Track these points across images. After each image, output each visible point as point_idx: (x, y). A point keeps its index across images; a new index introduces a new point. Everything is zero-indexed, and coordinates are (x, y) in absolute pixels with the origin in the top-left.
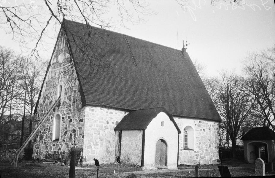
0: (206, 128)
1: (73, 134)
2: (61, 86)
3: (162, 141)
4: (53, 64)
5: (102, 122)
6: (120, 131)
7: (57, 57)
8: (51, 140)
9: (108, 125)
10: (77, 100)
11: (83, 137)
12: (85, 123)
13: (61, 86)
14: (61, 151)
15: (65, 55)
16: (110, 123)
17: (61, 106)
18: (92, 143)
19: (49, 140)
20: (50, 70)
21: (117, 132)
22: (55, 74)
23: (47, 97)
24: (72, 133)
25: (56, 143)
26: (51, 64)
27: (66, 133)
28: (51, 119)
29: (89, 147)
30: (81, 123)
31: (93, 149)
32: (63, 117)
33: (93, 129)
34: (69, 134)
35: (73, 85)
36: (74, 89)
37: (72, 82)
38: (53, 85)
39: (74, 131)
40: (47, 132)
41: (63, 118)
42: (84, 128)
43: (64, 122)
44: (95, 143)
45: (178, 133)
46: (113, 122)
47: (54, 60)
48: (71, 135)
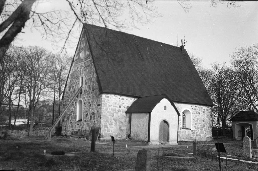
0: (201, 112)
1: (93, 116)
2: (82, 77)
3: (165, 122)
4: (76, 60)
5: (116, 107)
6: (130, 114)
7: (79, 54)
8: (76, 121)
9: (121, 109)
10: (95, 89)
11: (101, 118)
12: (102, 108)
13: (82, 77)
14: (83, 129)
15: (85, 53)
16: (122, 107)
17: (82, 94)
18: (108, 123)
19: (74, 121)
20: (73, 65)
21: (128, 115)
22: (78, 68)
23: (71, 86)
24: (91, 115)
25: (79, 123)
26: (75, 60)
27: (87, 115)
28: (75, 104)
29: (106, 126)
30: (99, 107)
31: (109, 128)
32: (85, 102)
33: (108, 112)
34: (89, 115)
35: (92, 77)
36: (93, 80)
37: (91, 74)
38: (76, 77)
39: (93, 114)
40: (72, 114)
41: (85, 103)
42: (101, 111)
43: (85, 107)
44: (110, 123)
45: (177, 116)
46: (124, 106)
47: (76, 56)
48: (91, 117)
